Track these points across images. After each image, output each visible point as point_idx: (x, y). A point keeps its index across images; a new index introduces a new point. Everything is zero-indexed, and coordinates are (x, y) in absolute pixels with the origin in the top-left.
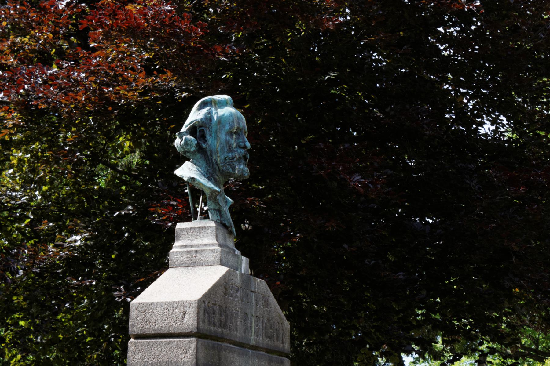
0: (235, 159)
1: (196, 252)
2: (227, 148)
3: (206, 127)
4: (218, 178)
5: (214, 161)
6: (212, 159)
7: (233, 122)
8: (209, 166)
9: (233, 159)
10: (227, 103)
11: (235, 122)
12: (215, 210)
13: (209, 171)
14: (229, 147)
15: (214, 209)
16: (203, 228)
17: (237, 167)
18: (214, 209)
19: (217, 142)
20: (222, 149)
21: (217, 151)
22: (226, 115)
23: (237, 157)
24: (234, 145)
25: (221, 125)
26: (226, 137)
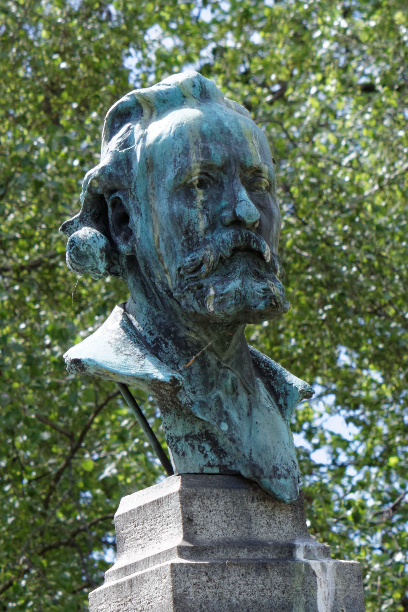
0: (205, 268)
1: (131, 582)
2: (179, 238)
3: (123, 190)
4: (193, 335)
5: (159, 287)
6: (154, 284)
7: (186, 152)
8: (156, 306)
9: (198, 268)
10: (184, 97)
11: (192, 152)
12: (195, 437)
13: (158, 321)
14: (186, 233)
15: (187, 437)
16: (158, 502)
17: (212, 292)
18: (187, 437)
19: (154, 231)
20: (170, 248)
21: (160, 255)
22: (164, 137)
23: (212, 259)
24: (202, 225)
25: (155, 173)
26: (171, 207)
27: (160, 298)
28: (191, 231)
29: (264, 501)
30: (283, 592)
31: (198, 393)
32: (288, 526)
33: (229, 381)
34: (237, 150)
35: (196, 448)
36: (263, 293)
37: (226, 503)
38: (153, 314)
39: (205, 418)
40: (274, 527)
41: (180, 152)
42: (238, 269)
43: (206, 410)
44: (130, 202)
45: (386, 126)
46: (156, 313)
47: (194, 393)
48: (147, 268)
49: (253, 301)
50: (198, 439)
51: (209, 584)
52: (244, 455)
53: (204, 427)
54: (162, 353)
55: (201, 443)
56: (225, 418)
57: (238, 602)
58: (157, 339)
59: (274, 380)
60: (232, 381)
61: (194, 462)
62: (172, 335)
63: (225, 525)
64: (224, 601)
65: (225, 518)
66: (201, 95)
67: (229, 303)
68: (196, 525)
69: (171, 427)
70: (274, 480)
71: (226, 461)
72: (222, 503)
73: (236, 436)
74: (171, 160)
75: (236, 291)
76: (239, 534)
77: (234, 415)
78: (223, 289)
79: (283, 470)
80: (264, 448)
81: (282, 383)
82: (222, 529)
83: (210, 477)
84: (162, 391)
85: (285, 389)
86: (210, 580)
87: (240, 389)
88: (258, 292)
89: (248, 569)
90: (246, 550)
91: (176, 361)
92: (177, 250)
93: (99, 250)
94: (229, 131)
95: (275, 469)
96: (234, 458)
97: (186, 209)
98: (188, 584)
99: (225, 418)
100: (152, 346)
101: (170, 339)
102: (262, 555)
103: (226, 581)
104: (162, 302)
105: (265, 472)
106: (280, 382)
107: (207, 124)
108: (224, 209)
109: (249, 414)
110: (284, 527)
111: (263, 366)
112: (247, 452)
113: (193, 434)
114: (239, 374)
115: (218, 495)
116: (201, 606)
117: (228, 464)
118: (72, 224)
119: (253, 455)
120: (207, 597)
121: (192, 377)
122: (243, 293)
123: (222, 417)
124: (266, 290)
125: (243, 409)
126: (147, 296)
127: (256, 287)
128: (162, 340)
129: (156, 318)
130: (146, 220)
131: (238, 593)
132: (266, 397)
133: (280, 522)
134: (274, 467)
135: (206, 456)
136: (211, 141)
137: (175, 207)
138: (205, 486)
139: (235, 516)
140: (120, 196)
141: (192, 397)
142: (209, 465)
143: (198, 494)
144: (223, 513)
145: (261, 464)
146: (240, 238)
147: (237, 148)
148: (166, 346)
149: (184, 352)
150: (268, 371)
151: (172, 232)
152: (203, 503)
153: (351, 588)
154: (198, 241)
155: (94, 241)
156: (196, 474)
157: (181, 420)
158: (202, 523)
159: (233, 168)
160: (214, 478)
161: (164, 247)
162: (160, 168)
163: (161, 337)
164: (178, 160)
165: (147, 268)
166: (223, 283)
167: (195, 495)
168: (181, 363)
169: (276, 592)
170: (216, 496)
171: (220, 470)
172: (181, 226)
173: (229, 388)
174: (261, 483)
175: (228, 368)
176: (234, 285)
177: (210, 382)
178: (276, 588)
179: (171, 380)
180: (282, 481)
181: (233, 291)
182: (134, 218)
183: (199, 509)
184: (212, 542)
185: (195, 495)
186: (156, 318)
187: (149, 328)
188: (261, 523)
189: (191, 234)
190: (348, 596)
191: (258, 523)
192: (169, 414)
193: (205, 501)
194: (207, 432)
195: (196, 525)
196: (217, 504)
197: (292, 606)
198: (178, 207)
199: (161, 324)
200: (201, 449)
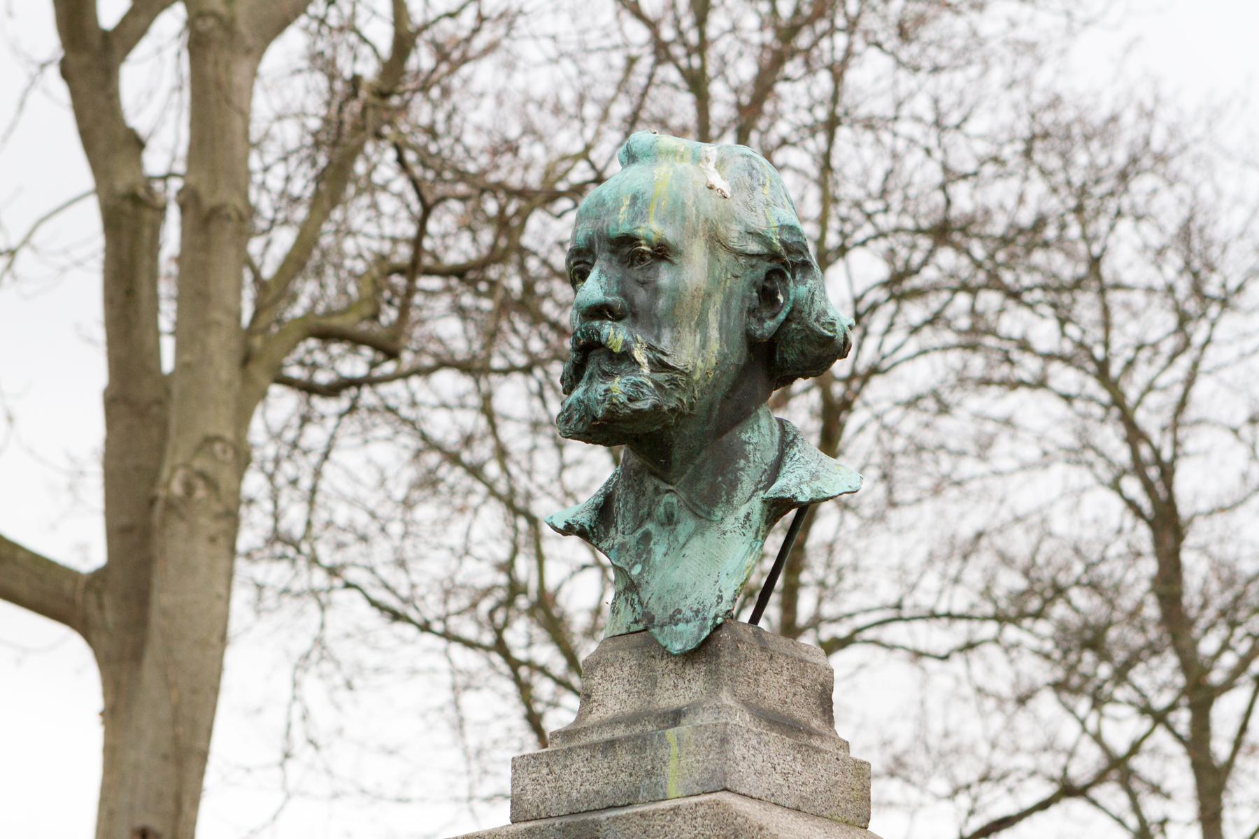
30: (631, 775)
32: (698, 683)
37: (631, 668)
40: (681, 688)
51: (550, 777)
57: (578, 795)
60: (665, 508)
63: (625, 696)
64: (564, 797)
65: (627, 687)
68: (595, 701)
86: (551, 773)
89: (594, 751)
90: (623, 725)
98: (527, 781)
102: (641, 728)
103: (567, 771)
110: (693, 686)
116: (538, 806)
120: (545, 794)
122: (586, 401)
131: (579, 783)
133: (689, 681)
143: (602, 661)
152: (605, 672)
153: (710, 757)
156: (622, 635)
169: (623, 775)
170: (621, 660)
173: (663, 518)
178: (622, 771)
179: (565, 526)
188: (667, 686)
190: (706, 769)
191: (663, 687)
193: (608, 670)
196: (621, 670)
197: (639, 791)
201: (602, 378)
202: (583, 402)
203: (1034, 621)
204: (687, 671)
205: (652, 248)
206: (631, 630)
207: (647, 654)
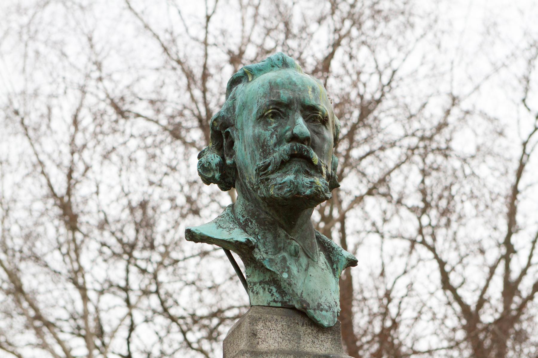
2: (259, 150)
6: (245, 183)
13: (248, 209)
14: (262, 147)
18: (260, 283)
26: (254, 131)
27: (249, 193)
28: (266, 146)
29: (311, 326)
31: (270, 253)
32: (328, 344)
33: (293, 248)
34: (299, 95)
35: (267, 289)
36: (310, 184)
37: (282, 325)
38: (246, 205)
39: (271, 269)
41: (261, 96)
42: (293, 169)
43: (274, 264)
44: (235, 133)
45: (358, 37)
46: (247, 204)
47: (267, 253)
48: (241, 174)
49: (303, 189)
50: (268, 284)
52: (297, 294)
53: (272, 276)
54: (248, 228)
55: (270, 286)
56: (287, 270)
58: (246, 220)
59: (332, 253)
61: (264, 298)
62: (256, 217)
63: (280, 340)
65: (281, 335)
66: (283, 65)
67: (286, 190)
68: (259, 338)
69: (250, 276)
70: (317, 311)
71: (286, 299)
72: (279, 325)
73: (293, 282)
74: (256, 101)
75: (291, 182)
76: (290, 346)
77: (294, 269)
78: (282, 180)
79: (325, 306)
80: (313, 291)
81: (337, 255)
82: (278, 342)
83: (274, 308)
84: (243, 250)
85: (338, 258)
87: (301, 253)
88: (306, 183)
90: (292, 356)
91: (257, 233)
92: (257, 159)
93: (214, 165)
94: (295, 83)
95: (319, 305)
96: (291, 296)
97: (263, 131)
99: (287, 270)
100: (243, 224)
101: (254, 219)
104: (250, 195)
105: (310, 306)
106: (336, 255)
107: (281, 79)
108: (287, 131)
109: (306, 270)
111: (327, 245)
112: (299, 293)
113: (265, 281)
114: (301, 244)
115: (277, 320)
117: (288, 300)
118: (204, 152)
119: (303, 294)
121: (266, 244)
122: (296, 184)
123: (285, 270)
124: (312, 183)
125: (302, 266)
126: (242, 193)
127: (305, 180)
128: (249, 220)
129: (247, 206)
130: (241, 143)
132: (323, 262)
134: (318, 303)
135: (272, 295)
136: (282, 89)
137: (256, 131)
138: (268, 313)
139: (289, 335)
140: (229, 130)
141: (265, 256)
142: (274, 301)
143: (262, 318)
144: (280, 332)
145: (309, 300)
146: (295, 148)
147: (300, 93)
148: (251, 224)
149: (263, 227)
150: (329, 248)
151: (254, 147)
152: (265, 324)
154: (270, 152)
155: (212, 159)
156: (264, 306)
157: (257, 271)
158: (263, 337)
159: (296, 105)
160: (277, 309)
161: (250, 158)
162: (250, 108)
163: (249, 218)
164: (260, 101)
165: (241, 174)
166: (282, 177)
167: (260, 318)
168: (260, 234)
170: (275, 320)
171: (282, 305)
172: (259, 143)
173: (293, 252)
174: (307, 312)
175: (294, 240)
176: (290, 177)
177: (279, 247)
179: (246, 241)
180: (324, 313)
181: (289, 181)
182: (236, 143)
183: (262, 328)
184: (269, 350)
185: (260, 318)
186: (247, 206)
187: (243, 213)
188: (308, 341)
189: (265, 148)
192: (249, 267)
193: (267, 323)
194: (273, 279)
195: (259, 338)
196: (276, 325)
198: (259, 130)
199: (250, 210)
200: (270, 291)
201: (304, 174)
202: (293, 183)
203: (179, 331)
204: (320, 335)
205: (323, 117)
206: (270, 305)
207: (293, 321)
